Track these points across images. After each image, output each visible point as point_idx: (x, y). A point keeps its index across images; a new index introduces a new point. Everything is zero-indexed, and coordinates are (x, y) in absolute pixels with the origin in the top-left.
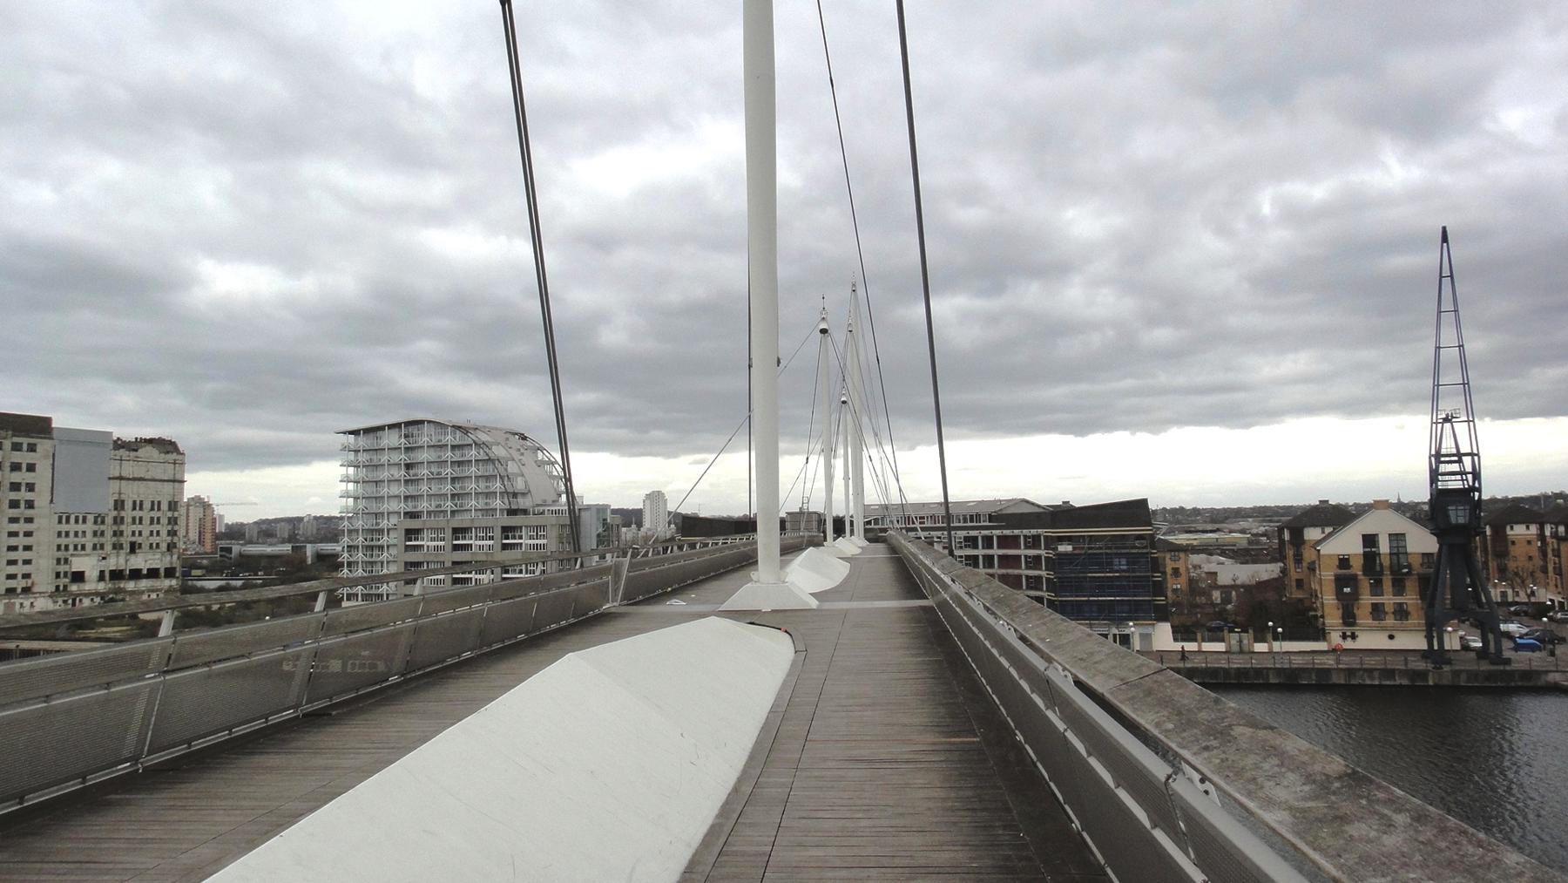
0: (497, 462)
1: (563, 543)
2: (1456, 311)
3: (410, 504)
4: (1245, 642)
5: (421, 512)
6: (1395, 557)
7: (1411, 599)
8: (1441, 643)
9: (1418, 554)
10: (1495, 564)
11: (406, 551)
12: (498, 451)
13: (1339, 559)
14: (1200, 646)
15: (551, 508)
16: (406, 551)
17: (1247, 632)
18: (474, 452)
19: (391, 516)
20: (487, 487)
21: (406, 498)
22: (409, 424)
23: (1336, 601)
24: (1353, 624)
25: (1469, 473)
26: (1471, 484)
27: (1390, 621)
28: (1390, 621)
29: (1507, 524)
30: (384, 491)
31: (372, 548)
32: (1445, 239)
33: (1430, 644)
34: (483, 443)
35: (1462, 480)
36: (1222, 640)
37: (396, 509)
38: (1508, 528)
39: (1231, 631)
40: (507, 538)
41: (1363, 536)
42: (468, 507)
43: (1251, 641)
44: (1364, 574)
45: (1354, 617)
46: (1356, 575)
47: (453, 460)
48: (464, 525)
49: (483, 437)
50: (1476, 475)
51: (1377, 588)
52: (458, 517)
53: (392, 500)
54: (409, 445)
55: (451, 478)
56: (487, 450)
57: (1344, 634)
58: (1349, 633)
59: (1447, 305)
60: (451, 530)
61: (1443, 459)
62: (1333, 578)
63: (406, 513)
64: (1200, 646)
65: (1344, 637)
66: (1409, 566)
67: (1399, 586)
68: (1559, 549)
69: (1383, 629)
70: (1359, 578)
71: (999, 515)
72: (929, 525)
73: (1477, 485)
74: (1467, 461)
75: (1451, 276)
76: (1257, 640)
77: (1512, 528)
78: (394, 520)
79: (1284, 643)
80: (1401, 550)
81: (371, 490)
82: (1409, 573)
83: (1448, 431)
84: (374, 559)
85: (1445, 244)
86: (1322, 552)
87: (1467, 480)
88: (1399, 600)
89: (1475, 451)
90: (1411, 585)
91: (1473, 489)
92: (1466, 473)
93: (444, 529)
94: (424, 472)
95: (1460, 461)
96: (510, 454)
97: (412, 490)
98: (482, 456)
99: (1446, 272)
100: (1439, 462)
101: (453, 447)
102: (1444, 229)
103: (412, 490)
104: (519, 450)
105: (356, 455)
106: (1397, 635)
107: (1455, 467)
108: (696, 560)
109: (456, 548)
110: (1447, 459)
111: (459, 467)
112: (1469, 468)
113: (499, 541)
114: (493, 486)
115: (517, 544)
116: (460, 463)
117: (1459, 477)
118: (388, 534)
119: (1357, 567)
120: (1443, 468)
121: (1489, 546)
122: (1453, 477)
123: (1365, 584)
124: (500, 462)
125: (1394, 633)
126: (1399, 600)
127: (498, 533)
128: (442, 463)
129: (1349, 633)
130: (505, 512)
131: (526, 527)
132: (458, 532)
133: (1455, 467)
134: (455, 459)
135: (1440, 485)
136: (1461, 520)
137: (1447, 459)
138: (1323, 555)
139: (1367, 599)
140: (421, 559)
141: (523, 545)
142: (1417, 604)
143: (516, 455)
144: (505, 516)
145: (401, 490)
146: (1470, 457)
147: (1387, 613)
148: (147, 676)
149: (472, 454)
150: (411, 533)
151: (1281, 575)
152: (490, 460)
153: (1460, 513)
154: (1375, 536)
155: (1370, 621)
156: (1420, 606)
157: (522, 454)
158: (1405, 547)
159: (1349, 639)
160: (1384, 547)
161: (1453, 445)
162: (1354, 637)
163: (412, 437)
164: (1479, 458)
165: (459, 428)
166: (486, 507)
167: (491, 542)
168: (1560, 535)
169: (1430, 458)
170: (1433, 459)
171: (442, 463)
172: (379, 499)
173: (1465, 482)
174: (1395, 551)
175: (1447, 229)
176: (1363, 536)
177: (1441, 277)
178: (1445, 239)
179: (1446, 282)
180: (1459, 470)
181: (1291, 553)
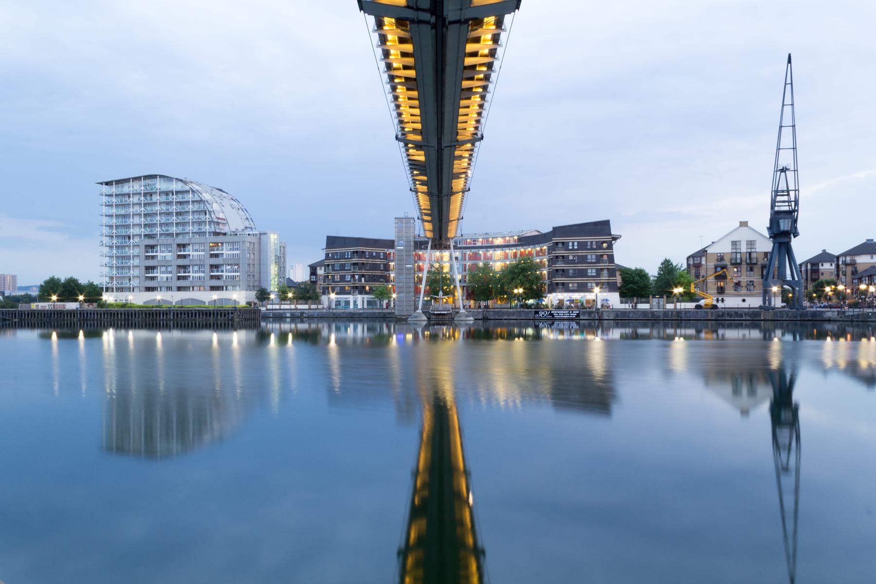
0: (206, 202)
1: (250, 253)
2: (792, 105)
3: (148, 229)
4: (661, 303)
5: (155, 234)
7: (756, 278)
8: (770, 303)
9: (762, 252)
10: (811, 285)
11: (146, 280)
12: (206, 196)
15: (241, 233)
16: (146, 280)
17: (663, 298)
18: (191, 195)
19: (135, 237)
20: (199, 229)
21: (145, 225)
23: (714, 280)
25: (793, 201)
26: (793, 208)
27: (744, 291)
28: (744, 291)
29: (820, 262)
30: (131, 221)
31: (123, 268)
32: (789, 61)
33: (764, 302)
34: (197, 190)
35: (789, 206)
36: (648, 302)
37: (139, 212)
38: (820, 265)
39: (654, 297)
41: (732, 242)
42: (187, 231)
43: (665, 302)
46: (727, 265)
47: (177, 200)
49: (196, 187)
50: (796, 202)
52: (180, 237)
53: (135, 268)
54: (147, 191)
55: (176, 223)
56: (200, 195)
57: (718, 299)
59: (788, 101)
61: (779, 194)
62: (714, 267)
63: (145, 235)
68: (846, 271)
70: (728, 266)
71: (521, 237)
73: (796, 208)
74: (792, 194)
75: (792, 84)
76: (668, 302)
77: (822, 265)
79: (683, 304)
83: (783, 180)
84: (124, 265)
85: (789, 65)
86: (708, 252)
87: (791, 206)
89: (797, 189)
90: (757, 270)
91: (794, 211)
92: (791, 202)
93: (171, 288)
94: (156, 198)
95: (788, 195)
96: (214, 199)
97: (149, 220)
98: (196, 198)
99: (789, 81)
100: (776, 195)
103: (149, 220)
104: (220, 197)
107: (786, 198)
109: (179, 257)
110: (781, 194)
111: (180, 205)
112: (793, 199)
113: (208, 273)
116: (181, 203)
117: (787, 204)
118: (133, 239)
120: (779, 198)
122: (784, 204)
124: (208, 203)
127: (207, 268)
128: (169, 214)
130: (212, 234)
131: (225, 243)
133: (786, 198)
134: (178, 200)
135: (776, 209)
137: (781, 194)
138: (710, 253)
140: (156, 285)
141: (224, 255)
142: (760, 281)
143: (218, 200)
144: (212, 236)
145: (143, 231)
146: (794, 192)
147: (742, 287)
148: (553, 266)
149: (190, 197)
152: (201, 201)
155: (733, 292)
156: (761, 283)
157: (222, 199)
161: (785, 185)
163: (149, 186)
164: (799, 191)
165: (181, 180)
166: (199, 231)
167: (238, 252)
168: (847, 262)
169: (772, 192)
170: (773, 192)
171: (169, 214)
172: (126, 205)
173: (790, 207)
175: (791, 55)
176: (732, 242)
177: (786, 84)
178: (789, 61)
180: (787, 199)
181: (693, 271)
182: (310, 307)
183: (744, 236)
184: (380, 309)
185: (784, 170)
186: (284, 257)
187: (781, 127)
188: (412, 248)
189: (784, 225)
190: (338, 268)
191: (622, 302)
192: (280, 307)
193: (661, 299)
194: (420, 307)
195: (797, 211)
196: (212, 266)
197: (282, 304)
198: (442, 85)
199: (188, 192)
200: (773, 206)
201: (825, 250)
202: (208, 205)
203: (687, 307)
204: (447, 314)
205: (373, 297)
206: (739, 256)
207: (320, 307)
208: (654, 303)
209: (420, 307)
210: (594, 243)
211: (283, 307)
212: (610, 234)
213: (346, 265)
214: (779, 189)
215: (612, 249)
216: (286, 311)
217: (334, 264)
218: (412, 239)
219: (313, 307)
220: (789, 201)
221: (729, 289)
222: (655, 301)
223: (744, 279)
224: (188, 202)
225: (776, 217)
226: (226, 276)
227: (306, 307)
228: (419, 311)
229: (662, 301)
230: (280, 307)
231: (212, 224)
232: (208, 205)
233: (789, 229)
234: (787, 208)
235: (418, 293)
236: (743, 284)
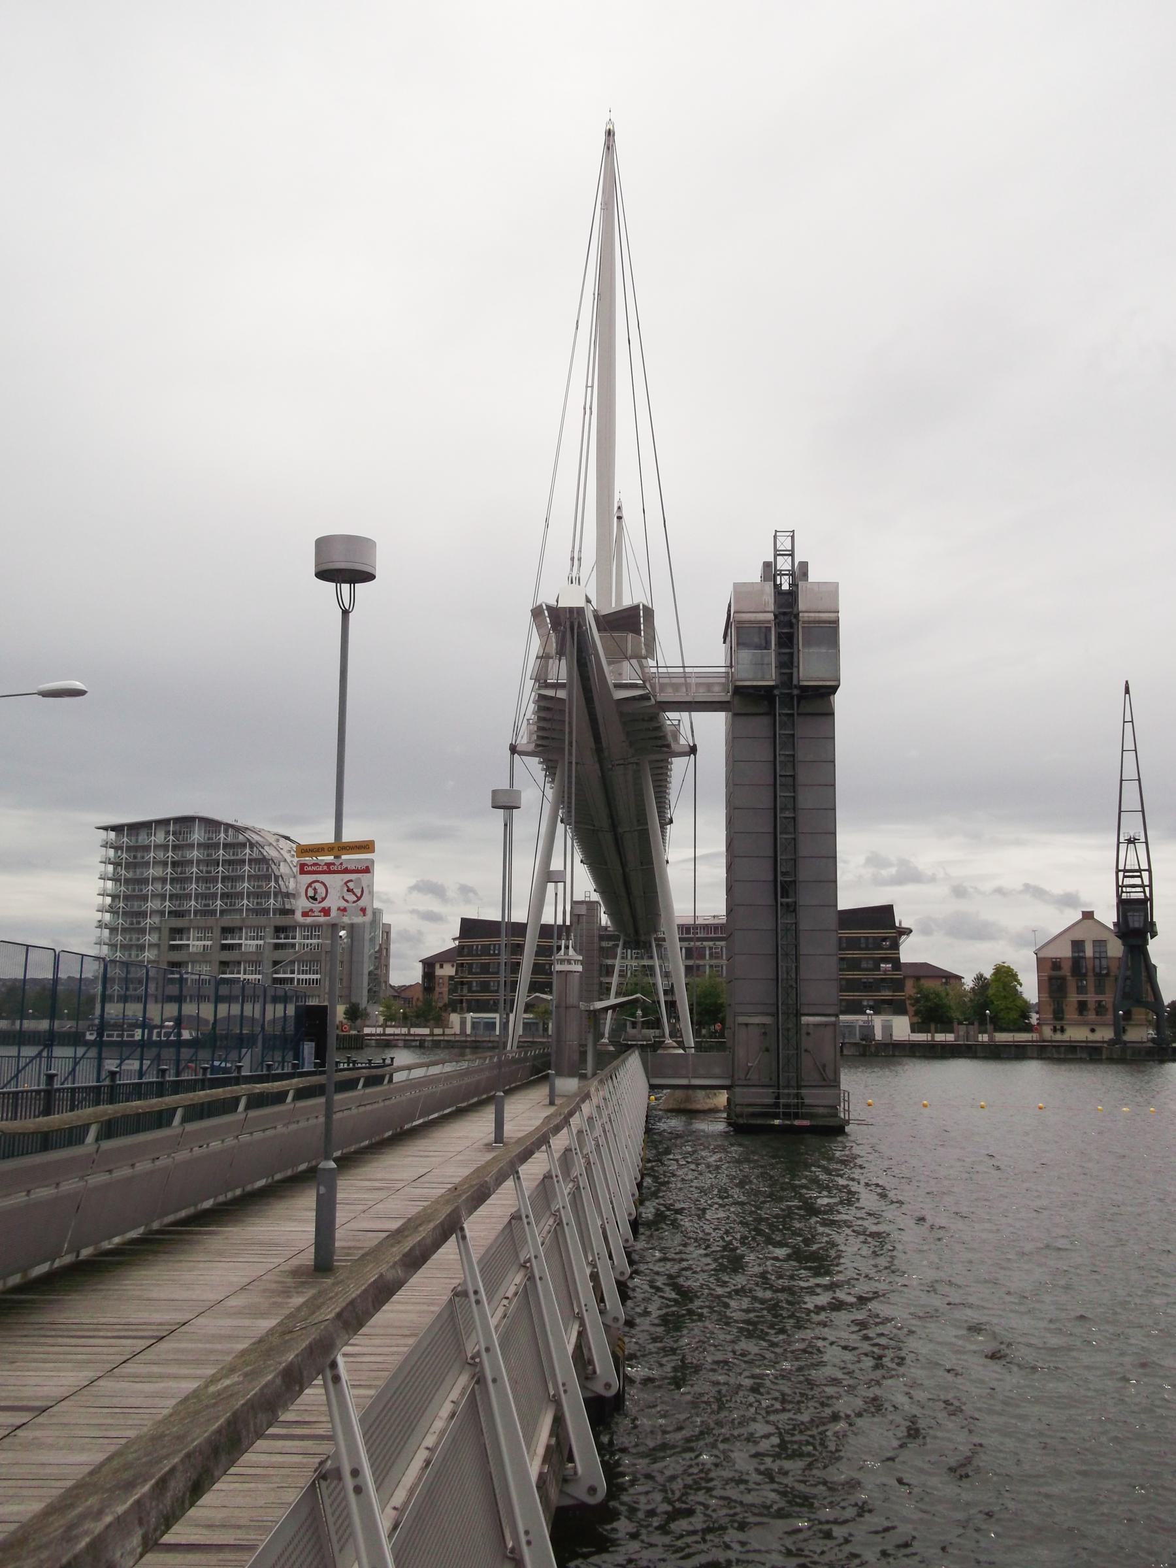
4: (972, 1033)
6: (1097, 961)
13: (1053, 962)
14: (933, 1037)
22: (177, 820)
24: (1062, 1019)
27: (1091, 1016)
28: (1091, 1016)
32: (1127, 691)
40: (278, 938)
41: (1073, 942)
44: (1073, 976)
45: (1062, 1012)
48: (231, 925)
51: (1081, 990)
57: (1055, 1027)
58: (1058, 1027)
60: (219, 929)
64: (933, 1037)
65: (1055, 1030)
66: (1108, 968)
67: (1100, 989)
69: (1085, 1024)
72: (702, 936)
74: (1145, 875)
78: (156, 920)
80: (1103, 955)
81: (660, 771)
82: (1107, 975)
88: (1100, 998)
95: (1140, 876)
101: (226, 846)
102: (1127, 682)
105: (116, 852)
106: (1098, 1028)
108: (280, 1129)
109: (225, 947)
114: (267, 885)
115: (289, 944)
119: (1066, 970)
121: (575, 695)
123: (1072, 984)
125: (1094, 1027)
126: (1100, 998)
129: (1058, 1027)
132: (227, 931)
133: (1138, 881)
135: (1124, 896)
136: (1137, 925)
139: (1073, 998)
150: (177, 932)
151: (1030, 988)
153: (1136, 918)
154: (1083, 942)
158: (1106, 952)
159: (1059, 1032)
160: (1089, 952)
162: (1062, 1030)
174: (1097, 955)
176: (1073, 942)
178: (1127, 691)
179: (1128, 726)
182: (432, 1031)
183: (1088, 935)
184: (543, 1037)
185: (1131, 841)
186: (387, 949)
187: (1122, 780)
188: (596, 974)
189: (1136, 922)
190: (478, 970)
191: (913, 1031)
192: (384, 1030)
193: (971, 1027)
194: (607, 1035)
195: (1151, 899)
196: (275, 963)
197: (387, 1026)
198: (620, 854)
199: (243, 845)
200: (1119, 896)
201: (982, 976)
202: (273, 866)
203: (1016, 1039)
204: (647, 1045)
205: (531, 1016)
206: (1104, 962)
207: (448, 1031)
208: (961, 1033)
209: (607, 1035)
210: (871, 941)
211: (389, 1031)
212: (893, 926)
213: (491, 966)
214: (1127, 868)
215: (898, 950)
216: (396, 1037)
217: (472, 964)
218: (596, 932)
219: (437, 1031)
220: (1143, 886)
221: (1071, 1014)
222: (962, 1030)
223: (1091, 998)
224: (243, 861)
225: (1125, 905)
226: (298, 980)
227: (426, 1031)
228: (605, 1040)
229: (973, 1029)
230: (384, 1030)
231: (280, 896)
232: (273, 866)
233: (1142, 925)
234: (1141, 896)
235: (865, 987)
236: (1092, 1005)
